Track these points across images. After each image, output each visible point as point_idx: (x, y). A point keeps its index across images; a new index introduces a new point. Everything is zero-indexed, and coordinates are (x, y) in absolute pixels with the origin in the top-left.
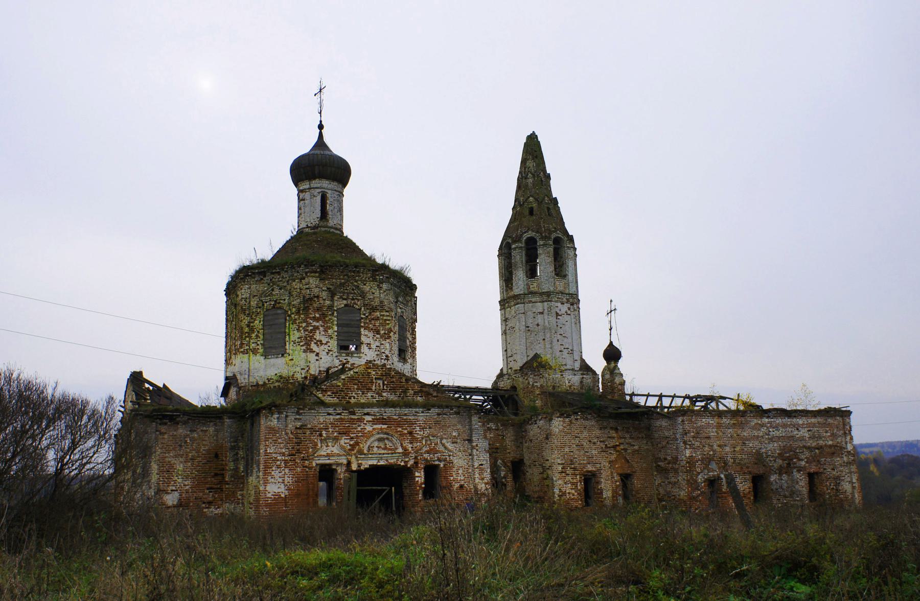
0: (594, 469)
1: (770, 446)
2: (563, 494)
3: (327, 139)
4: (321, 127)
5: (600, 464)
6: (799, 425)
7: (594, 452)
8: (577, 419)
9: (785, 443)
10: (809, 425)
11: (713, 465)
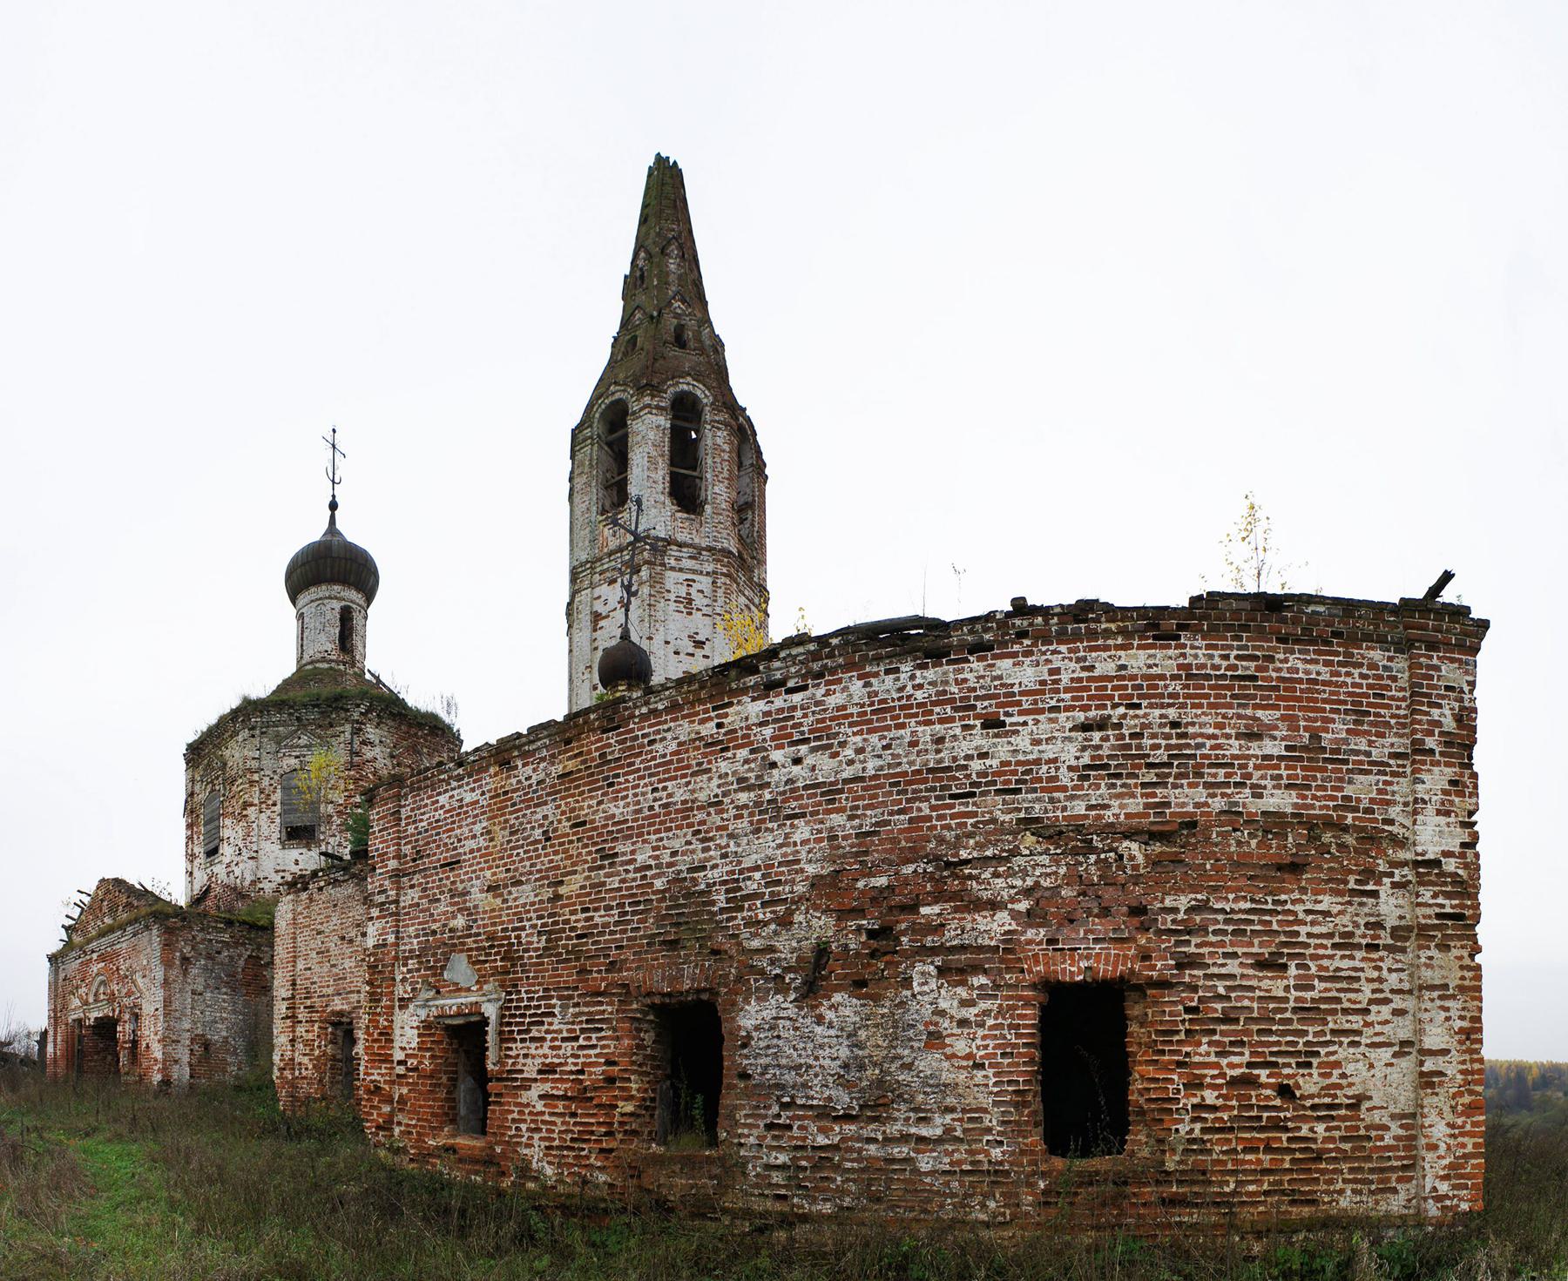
0: (345, 1007)
1: (766, 846)
2: (291, 1064)
3: (339, 526)
4: (333, 506)
5: (359, 992)
6: (1009, 698)
7: (348, 964)
8: (320, 889)
9: (870, 818)
10: (1090, 689)
11: (460, 970)
